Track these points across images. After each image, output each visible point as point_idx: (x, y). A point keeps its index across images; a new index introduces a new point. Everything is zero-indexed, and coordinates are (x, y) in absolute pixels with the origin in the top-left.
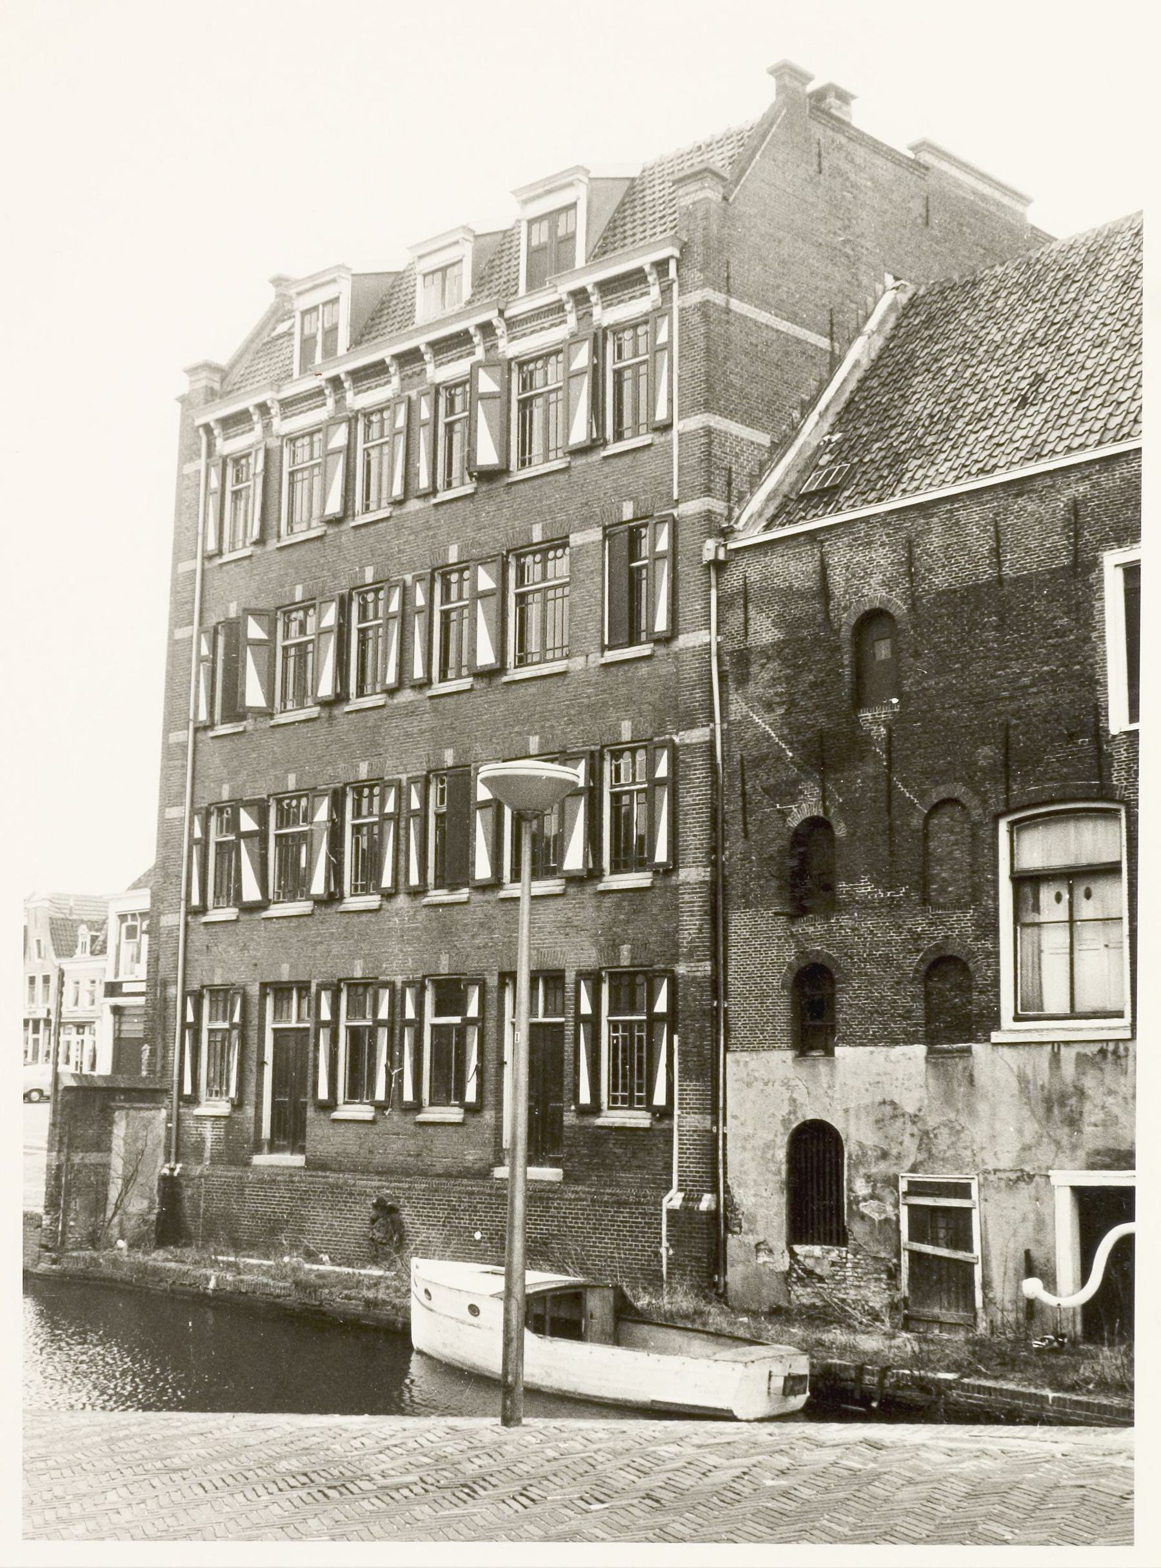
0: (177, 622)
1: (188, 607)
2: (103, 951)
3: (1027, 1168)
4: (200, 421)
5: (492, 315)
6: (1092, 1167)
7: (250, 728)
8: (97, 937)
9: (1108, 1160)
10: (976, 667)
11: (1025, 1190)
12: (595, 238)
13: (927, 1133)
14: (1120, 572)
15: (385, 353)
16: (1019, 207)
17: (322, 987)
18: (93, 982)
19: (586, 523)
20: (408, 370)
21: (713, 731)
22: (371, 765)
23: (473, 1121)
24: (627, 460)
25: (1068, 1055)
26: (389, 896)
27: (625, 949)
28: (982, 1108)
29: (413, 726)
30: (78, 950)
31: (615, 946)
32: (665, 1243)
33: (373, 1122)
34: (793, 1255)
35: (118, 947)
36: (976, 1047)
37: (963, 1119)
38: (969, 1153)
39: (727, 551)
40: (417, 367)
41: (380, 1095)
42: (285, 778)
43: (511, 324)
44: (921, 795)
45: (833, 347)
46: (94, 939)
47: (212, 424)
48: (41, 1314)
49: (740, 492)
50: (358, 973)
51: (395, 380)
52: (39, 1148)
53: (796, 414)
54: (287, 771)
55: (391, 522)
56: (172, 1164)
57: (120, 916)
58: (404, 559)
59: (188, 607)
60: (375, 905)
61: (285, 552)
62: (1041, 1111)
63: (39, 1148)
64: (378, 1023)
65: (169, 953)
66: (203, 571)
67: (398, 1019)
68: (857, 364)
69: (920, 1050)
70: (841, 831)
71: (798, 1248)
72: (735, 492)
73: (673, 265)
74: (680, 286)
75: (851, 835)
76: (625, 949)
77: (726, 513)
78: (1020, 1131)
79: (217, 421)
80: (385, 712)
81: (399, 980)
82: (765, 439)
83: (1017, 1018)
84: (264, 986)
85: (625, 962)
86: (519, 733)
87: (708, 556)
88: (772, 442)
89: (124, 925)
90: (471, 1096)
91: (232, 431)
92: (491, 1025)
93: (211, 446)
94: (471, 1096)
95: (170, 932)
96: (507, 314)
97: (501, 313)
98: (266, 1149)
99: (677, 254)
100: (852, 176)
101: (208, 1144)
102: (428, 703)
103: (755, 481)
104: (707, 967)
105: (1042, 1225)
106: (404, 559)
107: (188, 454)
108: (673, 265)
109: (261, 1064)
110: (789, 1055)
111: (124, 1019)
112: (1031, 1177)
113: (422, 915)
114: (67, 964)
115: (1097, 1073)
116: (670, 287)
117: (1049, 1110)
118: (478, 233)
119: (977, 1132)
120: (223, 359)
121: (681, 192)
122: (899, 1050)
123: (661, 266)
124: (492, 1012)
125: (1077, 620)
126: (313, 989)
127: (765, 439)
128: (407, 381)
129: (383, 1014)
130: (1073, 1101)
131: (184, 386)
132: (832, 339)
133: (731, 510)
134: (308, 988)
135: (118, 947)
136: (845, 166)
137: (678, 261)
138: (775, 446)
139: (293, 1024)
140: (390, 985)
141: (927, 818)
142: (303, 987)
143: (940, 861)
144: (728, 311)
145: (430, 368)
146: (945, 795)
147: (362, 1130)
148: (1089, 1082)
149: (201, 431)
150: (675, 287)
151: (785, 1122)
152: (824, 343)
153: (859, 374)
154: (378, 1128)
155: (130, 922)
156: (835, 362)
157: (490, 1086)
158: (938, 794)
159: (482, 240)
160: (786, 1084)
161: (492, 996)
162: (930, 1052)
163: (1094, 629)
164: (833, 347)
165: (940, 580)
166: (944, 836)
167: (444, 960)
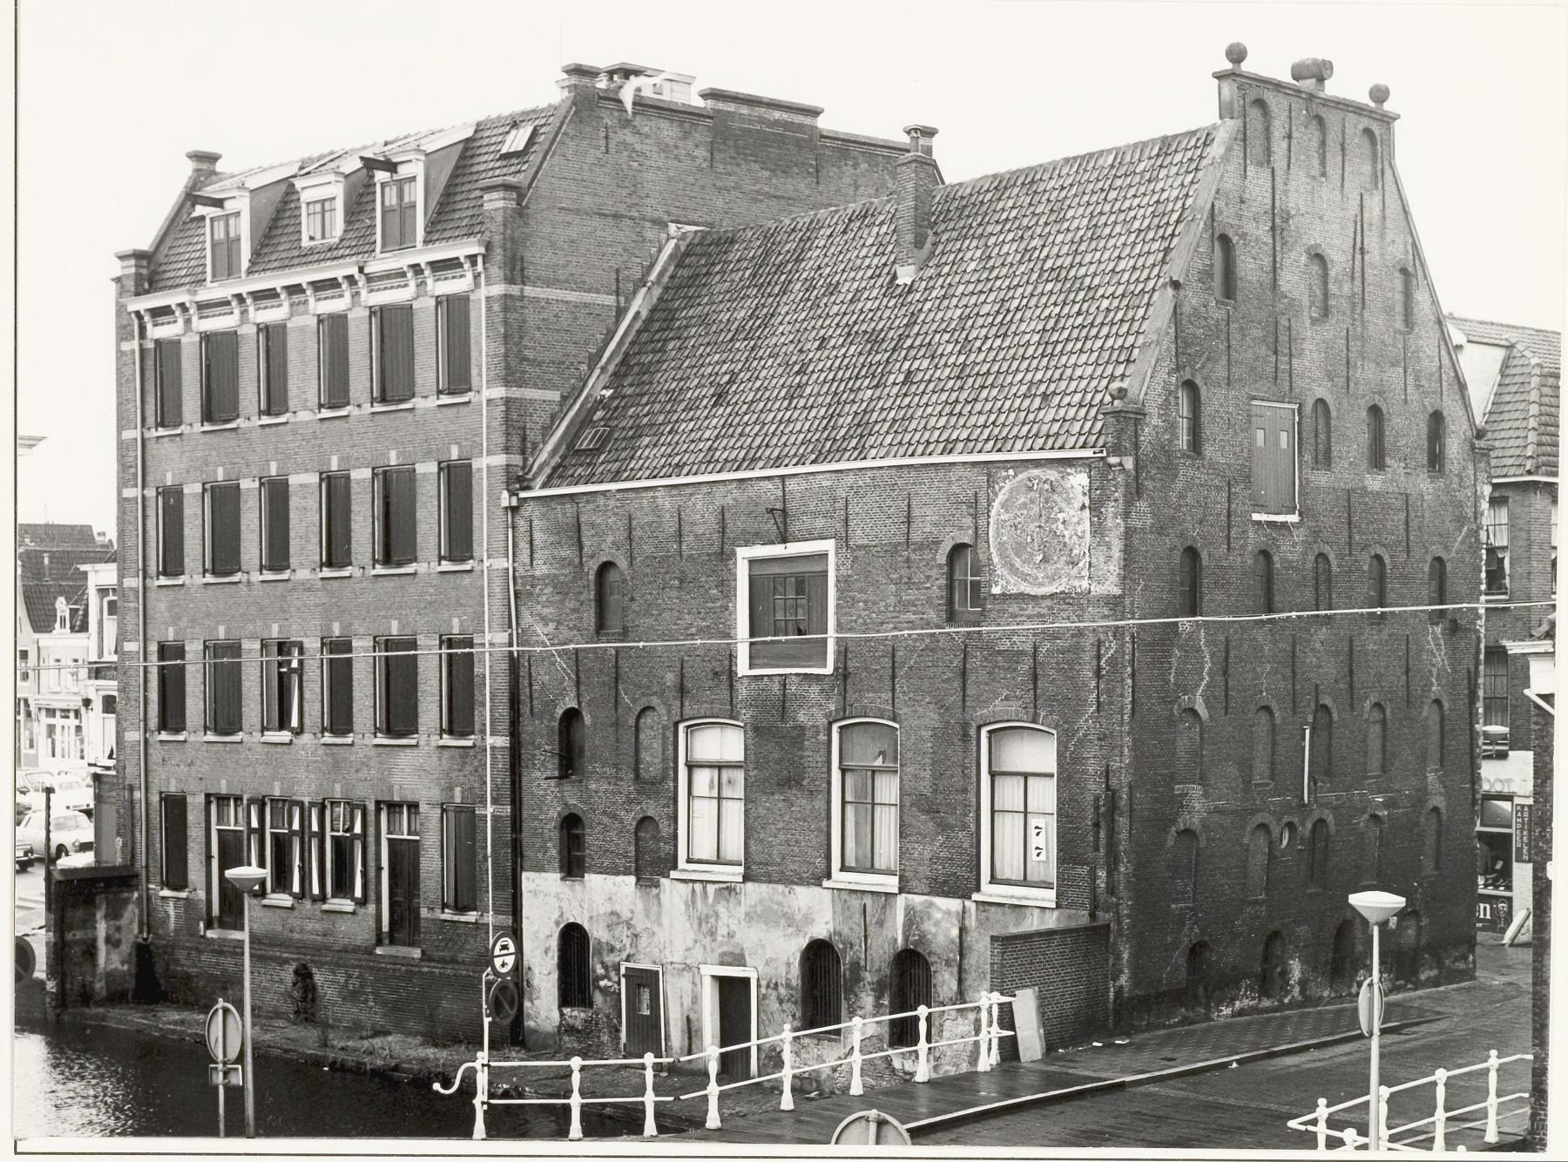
0: (123, 483)
1: (133, 470)
2: (84, 627)
3: (688, 962)
4: (132, 308)
5: (354, 271)
6: (722, 964)
7: (187, 583)
8: (77, 610)
9: (730, 960)
10: (666, 615)
11: (687, 976)
12: (433, 204)
13: (636, 936)
14: (746, 564)
15: (277, 281)
16: (808, 121)
17: (251, 801)
18: (76, 661)
19: (427, 455)
20: (296, 298)
21: (511, 635)
22: (280, 626)
23: (361, 911)
24: (454, 410)
25: (711, 888)
26: (299, 732)
27: (458, 790)
28: (665, 920)
29: (311, 600)
30: (57, 625)
31: (451, 789)
32: (485, 1006)
33: (292, 908)
34: (562, 1015)
35: (101, 623)
36: (663, 880)
37: (655, 928)
38: (657, 950)
39: (519, 499)
40: (301, 297)
41: (296, 888)
42: (216, 628)
43: (370, 279)
44: (634, 701)
45: (618, 301)
46: (73, 612)
47: (142, 313)
48: (48, 1043)
49: (534, 443)
50: (277, 793)
51: (286, 305)
52: (36, 902)
53: (584, 367)
54: (218, 623)
55: (289, 427)
56: (145, 935)
57: (99, 590)
58: (299, 461)
59: (133, 470)
60: (287, 740)
61: (208, 436)
62: (696, 926)
63: (36, 902)
64: (293, 833)
65: (134, 761)
66: (143, 440)
67: (307, 831)
68: (638, 314)
69: (632, 879)
70: (587, 719)
71: (567, 1011)
72: (529, 445)
73: (480, 260)
74: (486, 277)
75: (594, 724)
76: (458, 790)
77: (521, 464)
78: (685, 938)
79: (146, 310)
80: (289, 585)
81: (306, 800)
82: (555, 396)
83: (689, 861)
84: (378, 803)
85: (458, 800)
86: (385, 617)
87: (505, 503)
88: (562, 396)
89: (106, 600)
90: (358, 893)
91: (160, 320)
92: (371, 839)
93: (142, 329)
94: (358, 893)
95: (133, 747)
96: (367, 270)
97: (361, 270)
98: (216, 925)
99: (483, 250)
100: (638, 147)
101: (172, 919)
102: (320, 583)
103: (547, 431)
104: (508, 808)
105: (696, 1000)
106: (299, 461)
107: (123, 333)
108: (480, 260)
109: (379, 869)
110: (558, 876)
111: (103, 786)
112: (690, 968)
113: (321, 751)
114: (44, 639)
115: (725, 903)
116: (479, 274)
117: (700, 925)
118: (347, 172)
119: (662, 935)
120: (145, 244)
121: (486, 197)
122: (620, 878)
123: (472, 259)
124: (371, 830)
125: (722, 592)
126: (245, 802)
127: (555, 396)
128: (295, 308)
129: (296, 826)
130: (712, 920)
131: (117, 269)
132: (618, 295)
133: (525, 460)
134: (241, 799)
135: (101, 623)
136: (631, 139)
137: (484, 256)
138: (564, 398)
139: (232, 828)
140: (301, 804)
141: (638, 718)
142: (238, 799)
143: (646, 749)
144: (522, 298)
145: (312, 300)
146: (639, 709)
147: (284, 914)
148: (721, 909)
149: (133, 315)
150: (483, 276)
151: (558, 923)
152: (610, 300)
153: (638, 325)
154: (296, 913)
155: (112, 597)
156: (620, 312)
157: (372, 886)
158: (644, 702)
159: (353, 177)
160: (557, 896)
161: (371, 818)
162: (638, 880)
163: (731, 601)
164: (618, 301)
165: (648, 549)
166: (648, 732)
167: (338, 787)
